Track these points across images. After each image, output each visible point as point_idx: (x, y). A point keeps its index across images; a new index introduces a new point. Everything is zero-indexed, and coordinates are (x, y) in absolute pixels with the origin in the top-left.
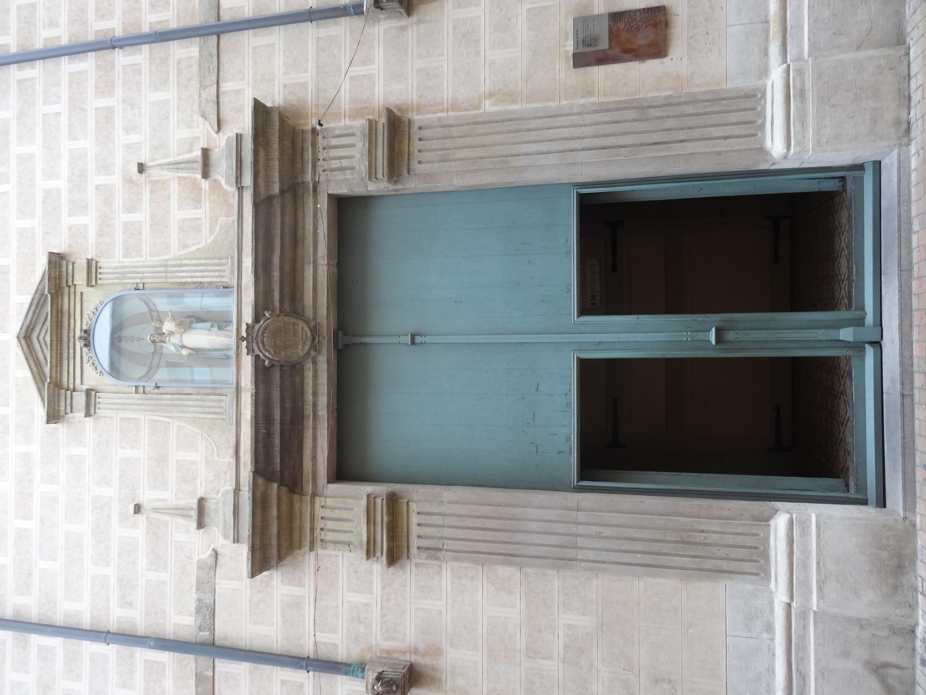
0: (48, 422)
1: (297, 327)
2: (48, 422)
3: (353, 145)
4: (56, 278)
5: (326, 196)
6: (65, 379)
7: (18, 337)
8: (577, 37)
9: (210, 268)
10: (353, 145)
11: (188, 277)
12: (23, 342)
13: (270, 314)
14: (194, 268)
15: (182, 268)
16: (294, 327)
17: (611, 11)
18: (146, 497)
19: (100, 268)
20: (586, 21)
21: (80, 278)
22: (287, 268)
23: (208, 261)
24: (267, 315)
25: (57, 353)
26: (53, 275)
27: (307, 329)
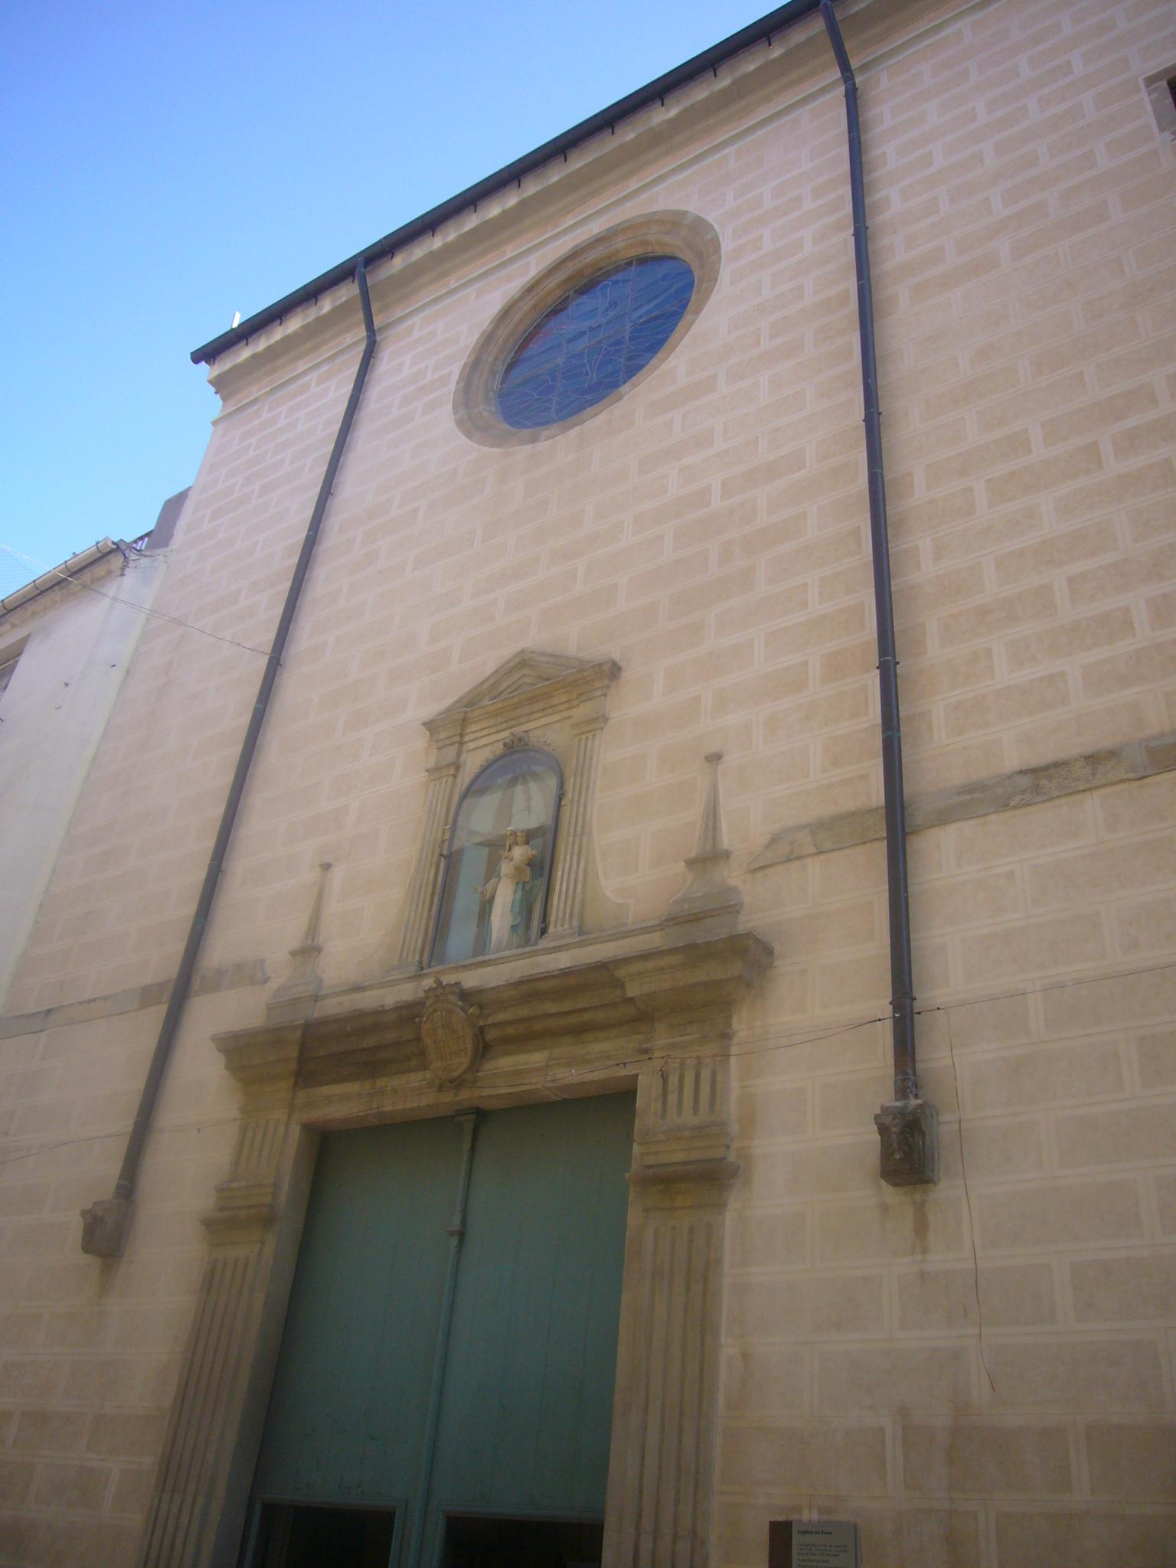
0: (424, 724)
1: (462, 1055)
2: (424, 724)
3: (696, 1110)
4: (584, 678)
5: (634, 1072)
6: (473, 728)
7: (522, 651)
8: (816, 1533)
9: (569, 902)
10: (696, 1110)
11: (563, 870)
12: (518, 659)
13: (472, 1014)
14: (573, 876)
15: (575, 858)
16: (462, 1050)
17: (606, 1526)
18: (338, 875)
19: (594, 736)
20: (846, 1551)
21: (582, 711)
22: (538, 1026)
23: (577, 900)
24: (471, 1010)
25: (501, 709)
26: (586, 674)
27: (460, 1071)
